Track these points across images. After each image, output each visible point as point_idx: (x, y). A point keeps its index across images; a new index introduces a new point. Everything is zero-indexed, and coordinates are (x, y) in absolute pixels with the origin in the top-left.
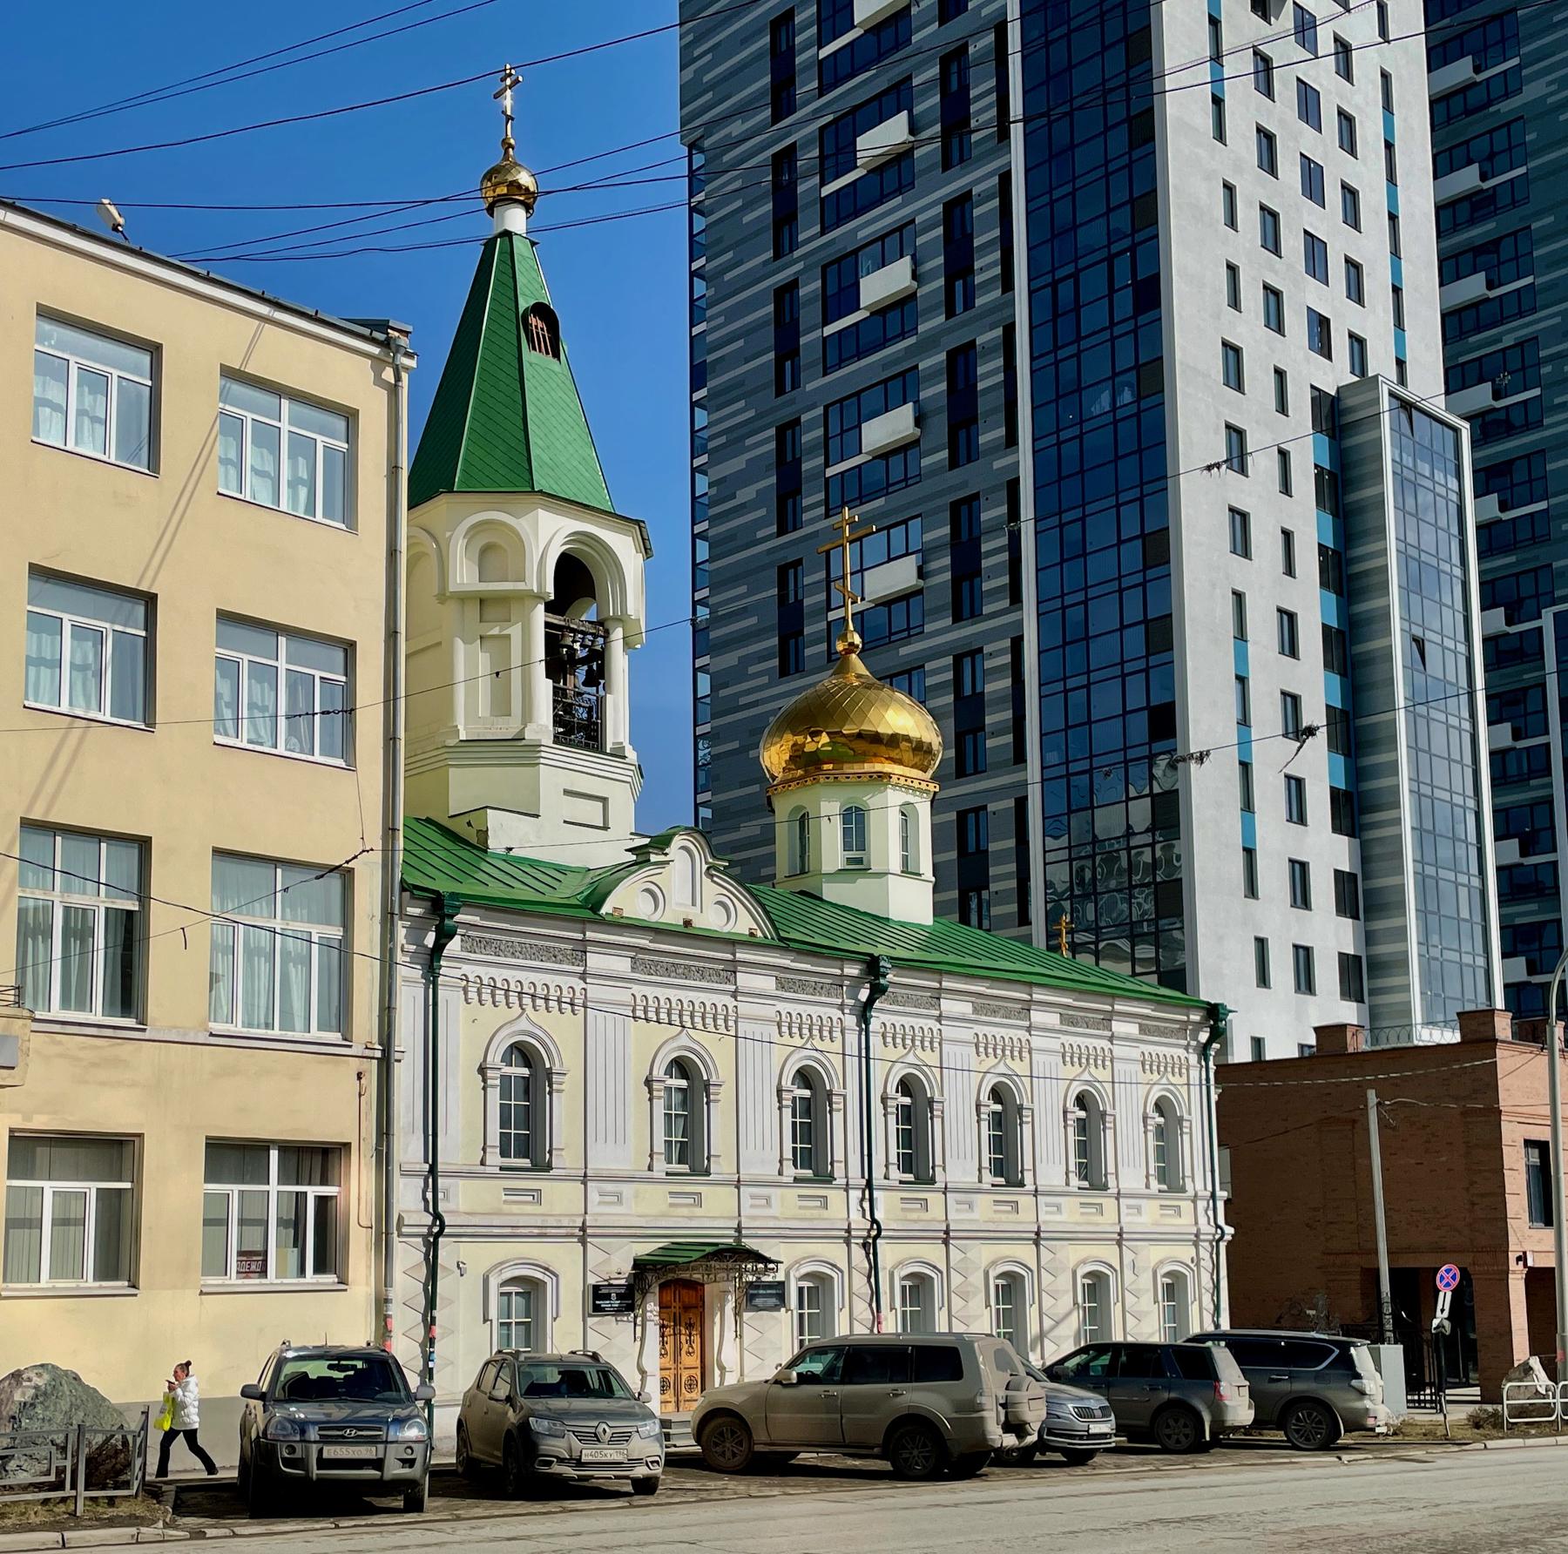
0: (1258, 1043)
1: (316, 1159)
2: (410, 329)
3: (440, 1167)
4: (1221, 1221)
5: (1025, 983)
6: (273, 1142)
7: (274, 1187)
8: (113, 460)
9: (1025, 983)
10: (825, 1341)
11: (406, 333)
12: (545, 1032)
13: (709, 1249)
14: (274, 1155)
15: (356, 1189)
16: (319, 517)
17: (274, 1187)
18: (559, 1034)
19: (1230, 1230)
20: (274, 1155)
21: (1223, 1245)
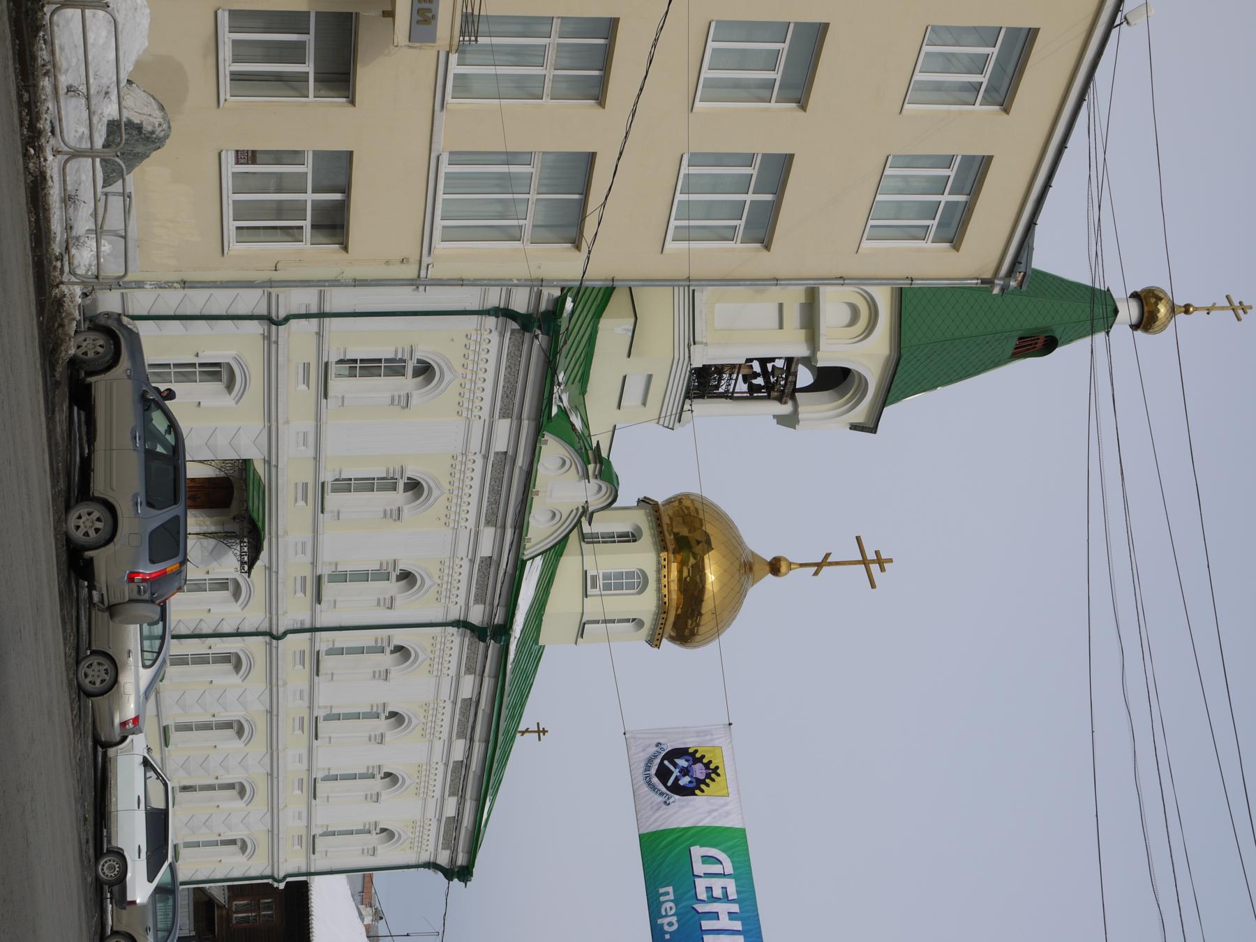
0: (877, 553)
1: (333, 224)
2: (1024, 288)
3: (327, 320)
4: (289, 879)
5: (1111, 25)
6: (349, 196)
7: (310, 197)
8: (915, 78)
9: (1111, 25)
10: (150, 908)
11: (1021, 284)
12: (443, 391)
13: (260, 524)
14: (338, 196)
15: (311, 255)
16: (871, 222)
17: (310, 197)
18: (447, 390)
19: (282, 886)
20: (338, 196)
21: (270, 881)
